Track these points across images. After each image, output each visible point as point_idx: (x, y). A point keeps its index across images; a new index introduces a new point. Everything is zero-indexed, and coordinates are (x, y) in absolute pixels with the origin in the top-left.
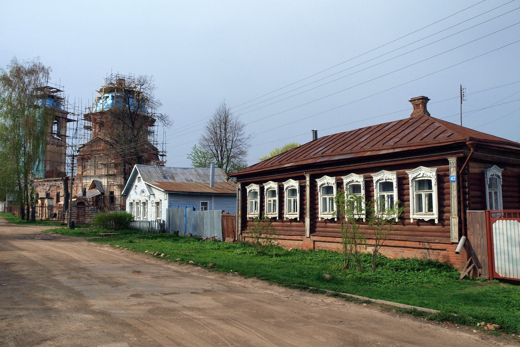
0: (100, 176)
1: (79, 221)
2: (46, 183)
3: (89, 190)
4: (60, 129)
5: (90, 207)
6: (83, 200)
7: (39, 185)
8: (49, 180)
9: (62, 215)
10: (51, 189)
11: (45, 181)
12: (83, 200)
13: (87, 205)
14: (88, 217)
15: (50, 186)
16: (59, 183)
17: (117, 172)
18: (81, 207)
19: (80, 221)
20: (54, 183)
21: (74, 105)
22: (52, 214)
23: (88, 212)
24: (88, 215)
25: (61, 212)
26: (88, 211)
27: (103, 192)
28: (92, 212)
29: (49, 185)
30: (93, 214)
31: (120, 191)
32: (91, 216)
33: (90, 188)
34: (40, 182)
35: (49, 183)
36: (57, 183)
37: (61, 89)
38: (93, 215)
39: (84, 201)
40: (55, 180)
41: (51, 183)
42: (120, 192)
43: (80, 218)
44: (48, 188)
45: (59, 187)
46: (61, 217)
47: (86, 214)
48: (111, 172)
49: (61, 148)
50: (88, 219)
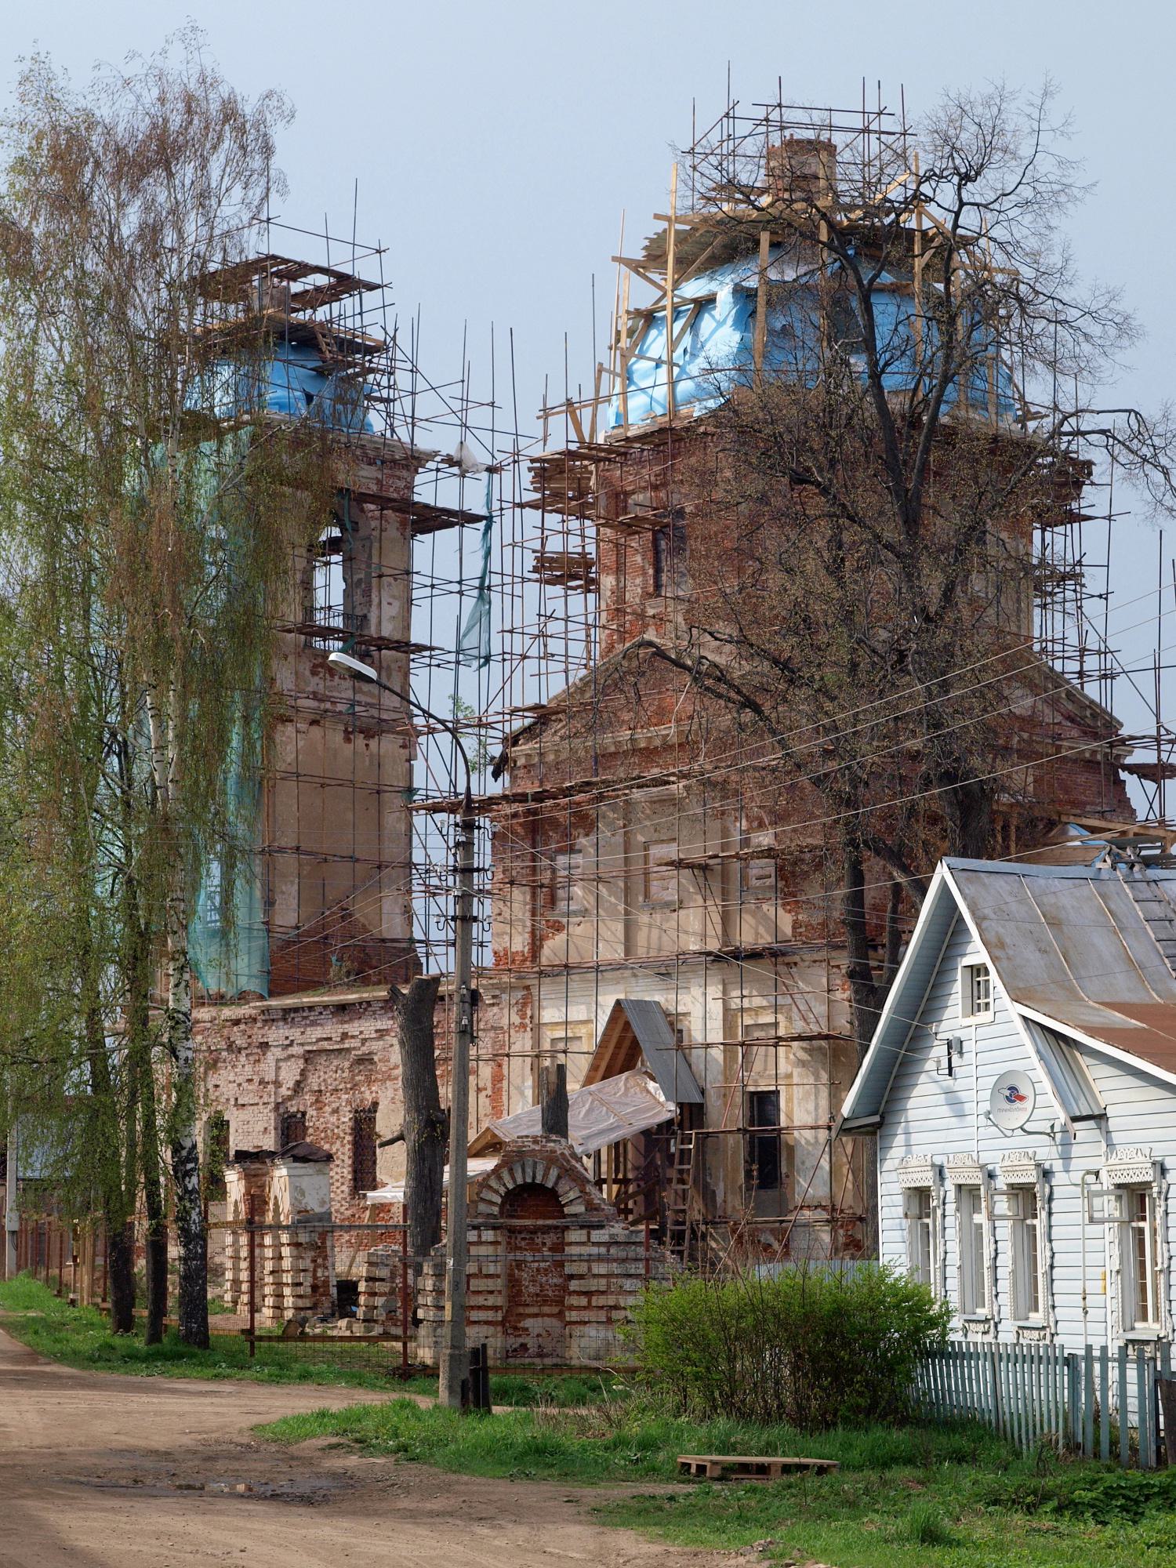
0: (670, 969)
1: (524, 1346)
2: (276, 1034)
3: (589, 1081)
4: (367, 593)
5: (601, 1227)
6: (546, 1175)
7: (230, 1047)
8: (296, 1010)
9: (392, 1292)
10: (314, 1082)
11: (270, 1018)
12: (546, 1175)
13: (580, 1209)
14: (586, 1315)
15: (309, 1057)
16: (366, 1027)
17: (796, 925)
18: (534, 1231)
19: (531, 1342)
20: (331, 1029)
21: (456, 390)
22: (326, 1283)
23: (582, 1268)
24: (588, 1294)
25: (384, 1273)
26: (590, 1259)
27: (698, 1099)
28: (615, 1268)
29: (296, 1050)
30: (628, 1284)
31: (824, 1092)
32: (611, 1300)
33: (594, 1068)
34: (237, 1022)
35: (295, 1033)
36: (353, 1028)
37: (366, 271)
38: (622, 1291)
39: (554, 1173)
40: (342, 1010)
41: (316, 1033)
42: (824, 1103)
43: (528, 1323)
44: (290, 1074)
45: (365, 1060)
46: (391, 1312)
47: (574, 1285)
48: (750, 933)
49: (373, 743)
50: (591, 1331)
